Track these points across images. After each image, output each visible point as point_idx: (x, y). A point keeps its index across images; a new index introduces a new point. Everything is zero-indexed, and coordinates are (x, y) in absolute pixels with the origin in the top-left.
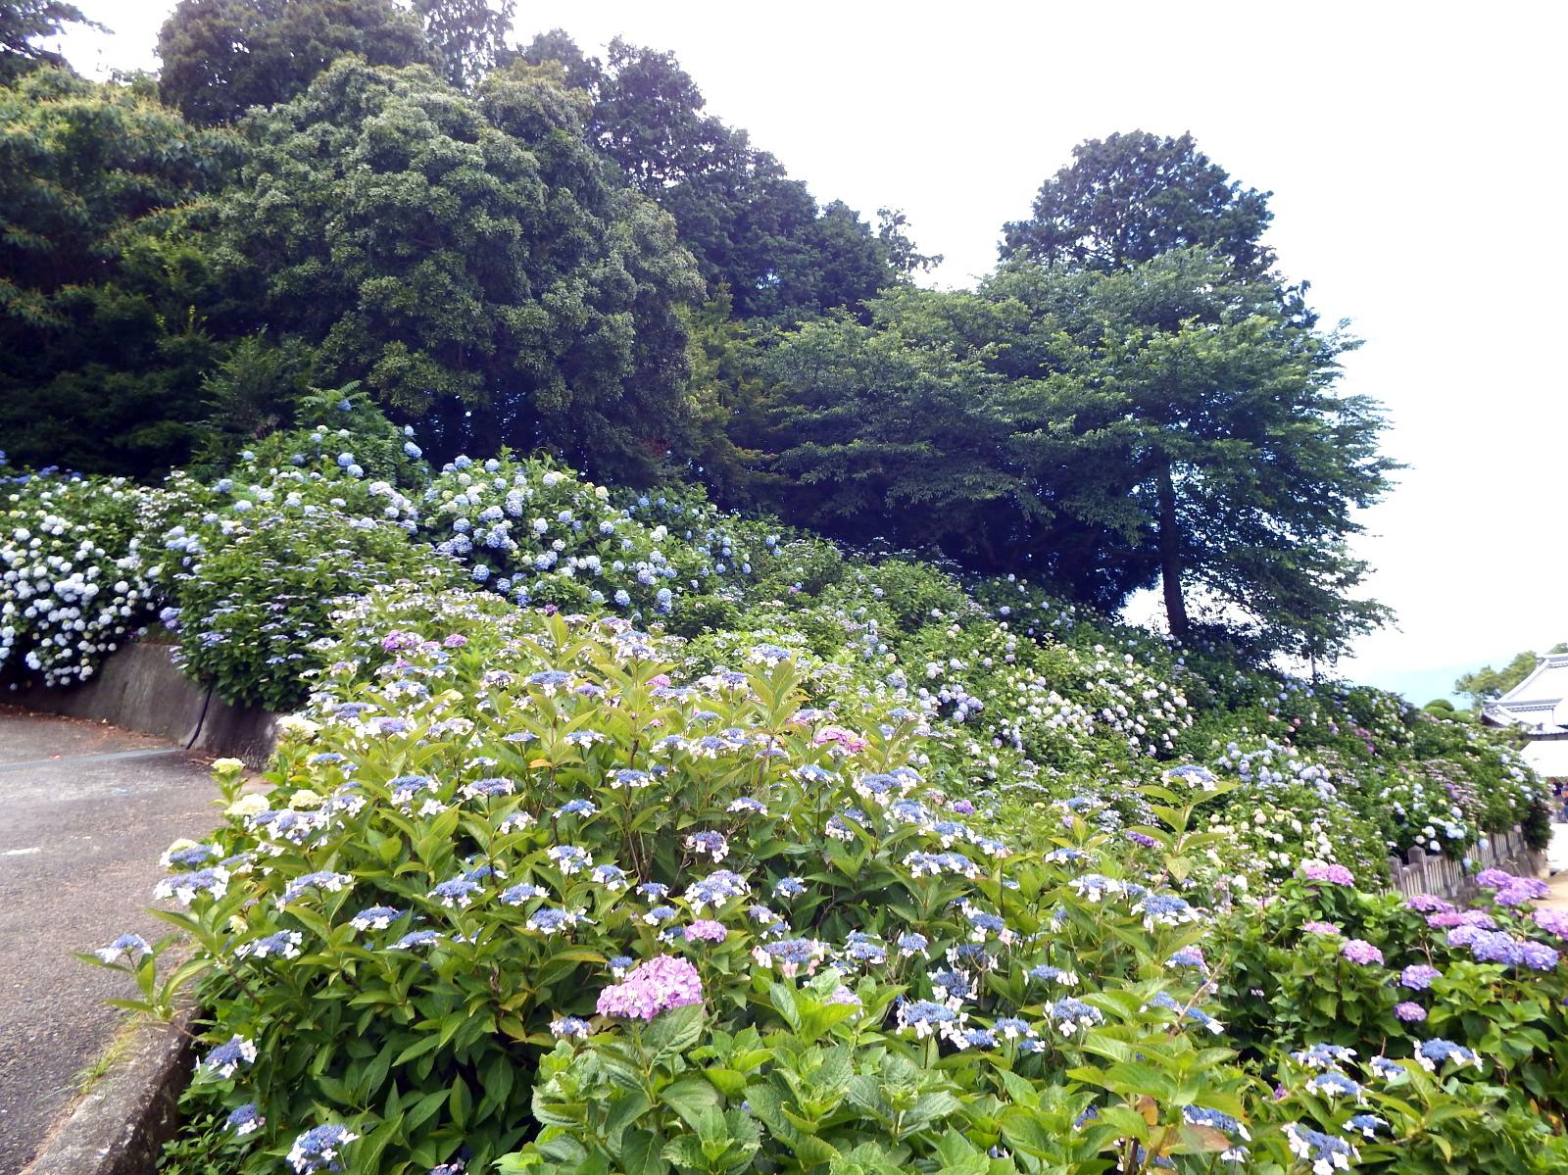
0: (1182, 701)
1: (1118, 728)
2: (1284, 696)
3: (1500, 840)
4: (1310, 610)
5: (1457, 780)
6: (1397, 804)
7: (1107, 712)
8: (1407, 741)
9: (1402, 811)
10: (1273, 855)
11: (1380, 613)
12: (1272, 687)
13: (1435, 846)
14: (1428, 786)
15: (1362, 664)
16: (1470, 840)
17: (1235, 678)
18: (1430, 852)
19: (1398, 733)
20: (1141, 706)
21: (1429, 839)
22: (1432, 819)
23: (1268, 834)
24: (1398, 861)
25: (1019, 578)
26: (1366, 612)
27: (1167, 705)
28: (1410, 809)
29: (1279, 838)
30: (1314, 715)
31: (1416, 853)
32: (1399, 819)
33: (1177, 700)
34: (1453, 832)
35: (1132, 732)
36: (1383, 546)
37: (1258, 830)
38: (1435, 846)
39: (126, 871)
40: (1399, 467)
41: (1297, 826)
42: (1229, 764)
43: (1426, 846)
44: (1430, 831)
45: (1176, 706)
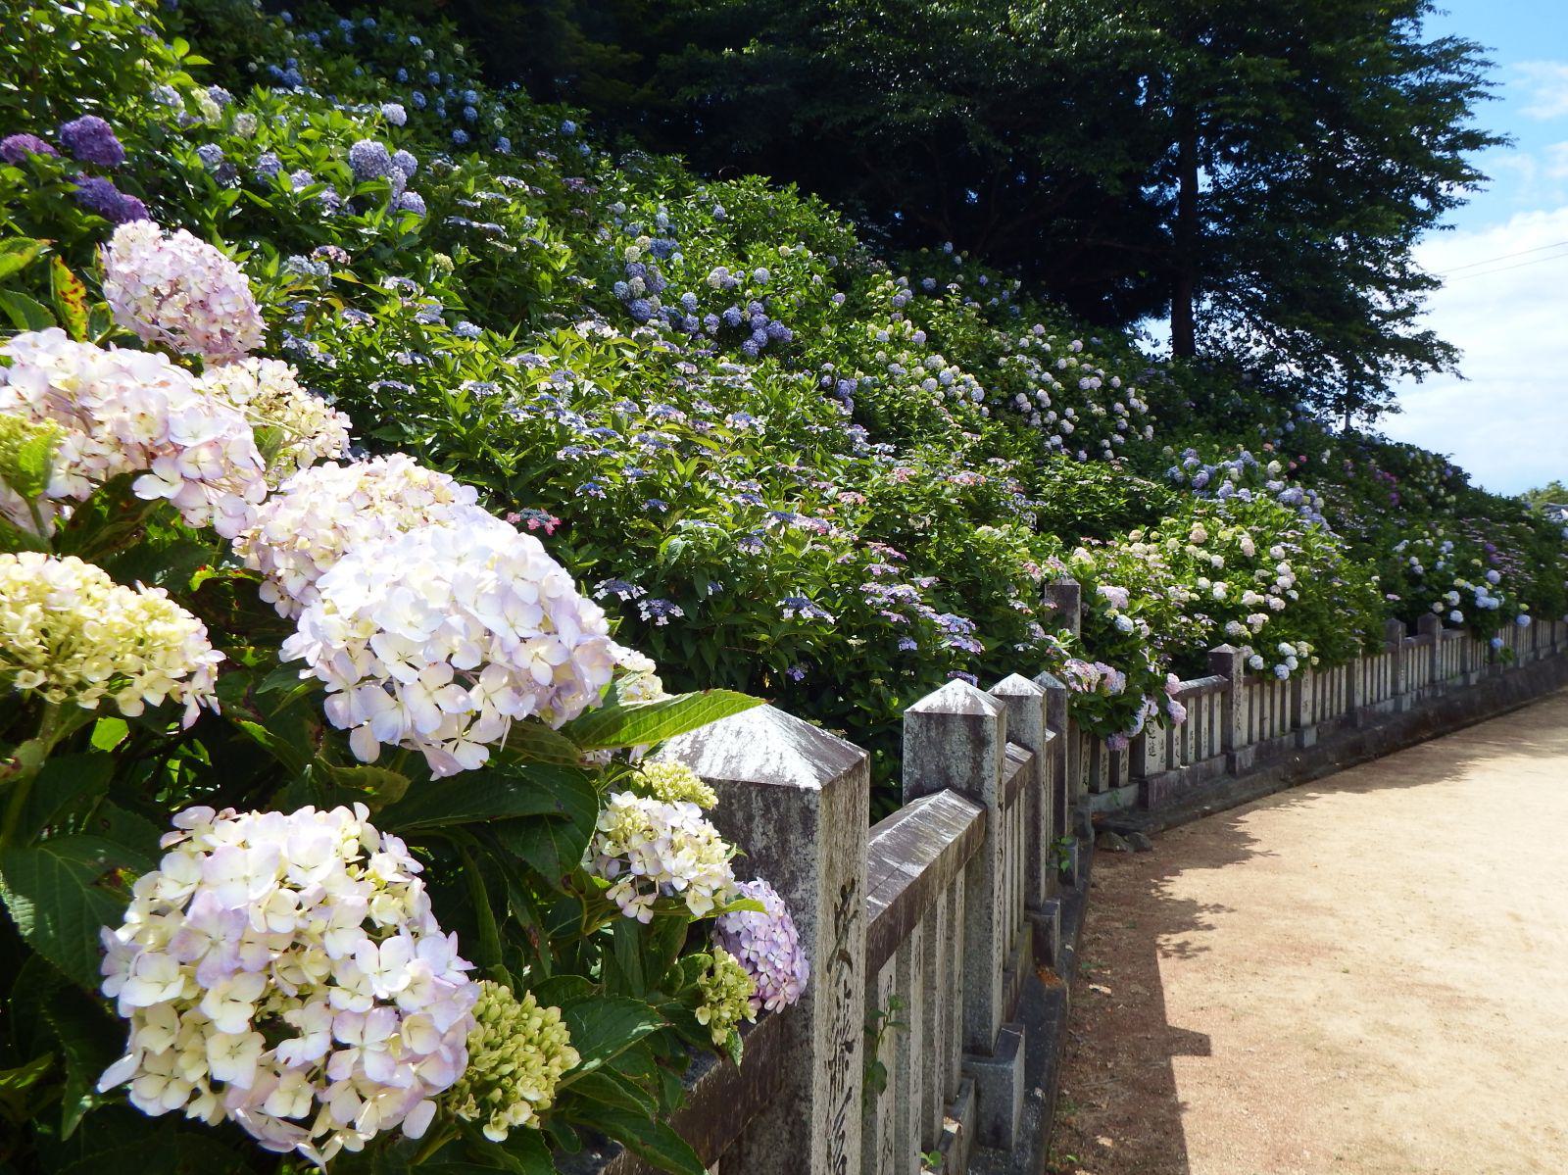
0: (1140, 405)
1: (1036, 421)
2: (1291, 426)
3: (1544, 630)
4: (1352, 326)
5: (1502, 546)
6: (1415, 560)
7: (1022, 398)
8: (1446, 505)
9: (1420, 569)
10: (1204, 582)
11: (1439, 353)
12: (1277, 412)
13: (1457, 616)
14: (1461, 543)
15: (1414, 414)
16: (1506, 616)
17: (1228, 397)
18: (1449, 624)
19: (1436, 494)
20: (1072, 395)
21: (1450, 607)
22: (1460, 582)
23: (1203, 554)
24: (1401, 627)
25: (957, 250)
26: (1425, 352)
27: (1119, 406)
28: (1431, 568)
29: (1218, 560)
30: (1328, 453)
31: (1429, 624)
32: (1413, 579)
33: (1134, 402)
34: (1485, 599)
35: (1056, 429)
36: (1465, 267)
37: (1190, 548)
38: (1457, 616)
39: (1226, 814)
40: (1498, 141)
41: (1247, 544)
42: (1179, 475)
43: (1445, 616)
44: (1454, 597)
45: (1131, 410)
